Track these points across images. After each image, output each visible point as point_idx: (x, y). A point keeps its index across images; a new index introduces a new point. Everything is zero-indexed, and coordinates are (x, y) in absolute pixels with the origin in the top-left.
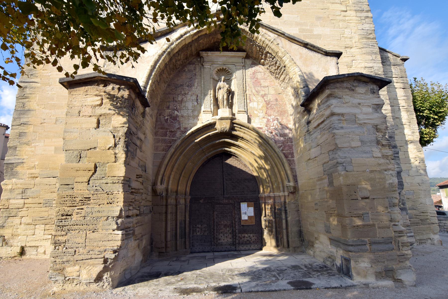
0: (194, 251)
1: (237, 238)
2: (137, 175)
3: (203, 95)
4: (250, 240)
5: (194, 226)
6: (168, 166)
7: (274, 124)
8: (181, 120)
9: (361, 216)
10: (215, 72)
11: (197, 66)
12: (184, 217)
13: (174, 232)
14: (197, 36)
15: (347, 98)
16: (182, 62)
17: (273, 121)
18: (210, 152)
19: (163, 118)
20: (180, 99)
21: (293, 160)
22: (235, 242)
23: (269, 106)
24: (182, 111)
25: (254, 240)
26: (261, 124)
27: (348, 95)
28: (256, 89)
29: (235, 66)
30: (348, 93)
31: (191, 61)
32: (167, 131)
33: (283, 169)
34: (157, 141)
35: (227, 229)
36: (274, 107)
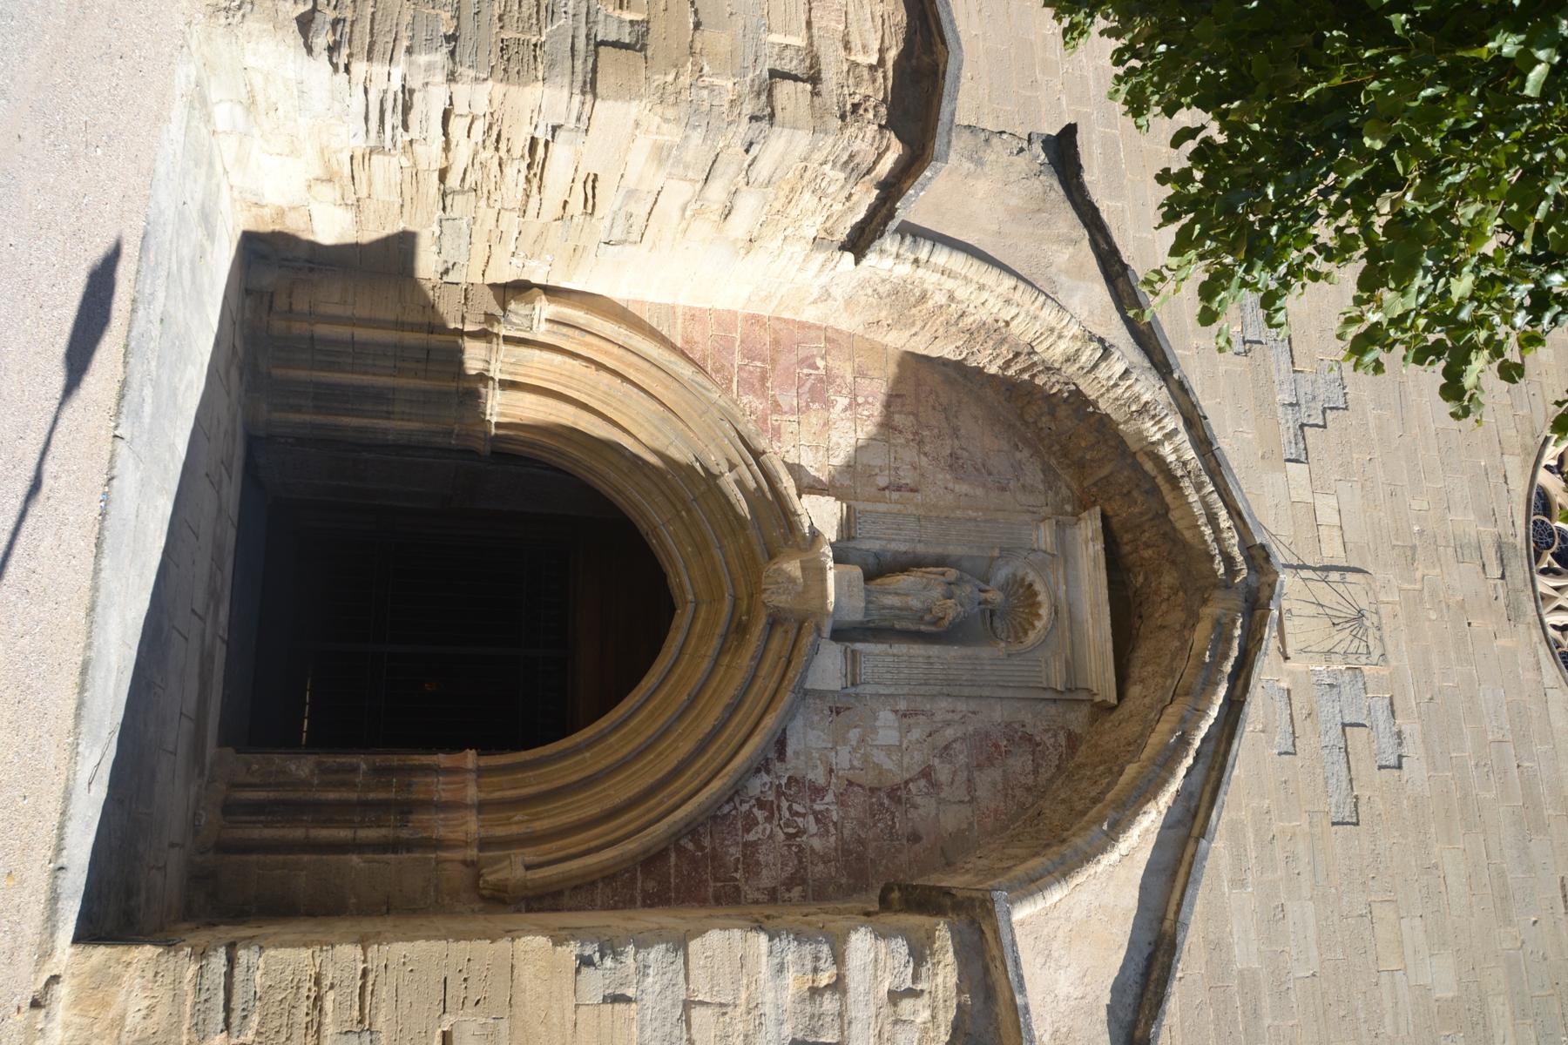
3: (921, 512)
7: (804, 815)
8: (814, 420)
11: (1042, 498)
17: (815, 813)
23: (886, 801)
32: (764, 361)
34: (725, 320)
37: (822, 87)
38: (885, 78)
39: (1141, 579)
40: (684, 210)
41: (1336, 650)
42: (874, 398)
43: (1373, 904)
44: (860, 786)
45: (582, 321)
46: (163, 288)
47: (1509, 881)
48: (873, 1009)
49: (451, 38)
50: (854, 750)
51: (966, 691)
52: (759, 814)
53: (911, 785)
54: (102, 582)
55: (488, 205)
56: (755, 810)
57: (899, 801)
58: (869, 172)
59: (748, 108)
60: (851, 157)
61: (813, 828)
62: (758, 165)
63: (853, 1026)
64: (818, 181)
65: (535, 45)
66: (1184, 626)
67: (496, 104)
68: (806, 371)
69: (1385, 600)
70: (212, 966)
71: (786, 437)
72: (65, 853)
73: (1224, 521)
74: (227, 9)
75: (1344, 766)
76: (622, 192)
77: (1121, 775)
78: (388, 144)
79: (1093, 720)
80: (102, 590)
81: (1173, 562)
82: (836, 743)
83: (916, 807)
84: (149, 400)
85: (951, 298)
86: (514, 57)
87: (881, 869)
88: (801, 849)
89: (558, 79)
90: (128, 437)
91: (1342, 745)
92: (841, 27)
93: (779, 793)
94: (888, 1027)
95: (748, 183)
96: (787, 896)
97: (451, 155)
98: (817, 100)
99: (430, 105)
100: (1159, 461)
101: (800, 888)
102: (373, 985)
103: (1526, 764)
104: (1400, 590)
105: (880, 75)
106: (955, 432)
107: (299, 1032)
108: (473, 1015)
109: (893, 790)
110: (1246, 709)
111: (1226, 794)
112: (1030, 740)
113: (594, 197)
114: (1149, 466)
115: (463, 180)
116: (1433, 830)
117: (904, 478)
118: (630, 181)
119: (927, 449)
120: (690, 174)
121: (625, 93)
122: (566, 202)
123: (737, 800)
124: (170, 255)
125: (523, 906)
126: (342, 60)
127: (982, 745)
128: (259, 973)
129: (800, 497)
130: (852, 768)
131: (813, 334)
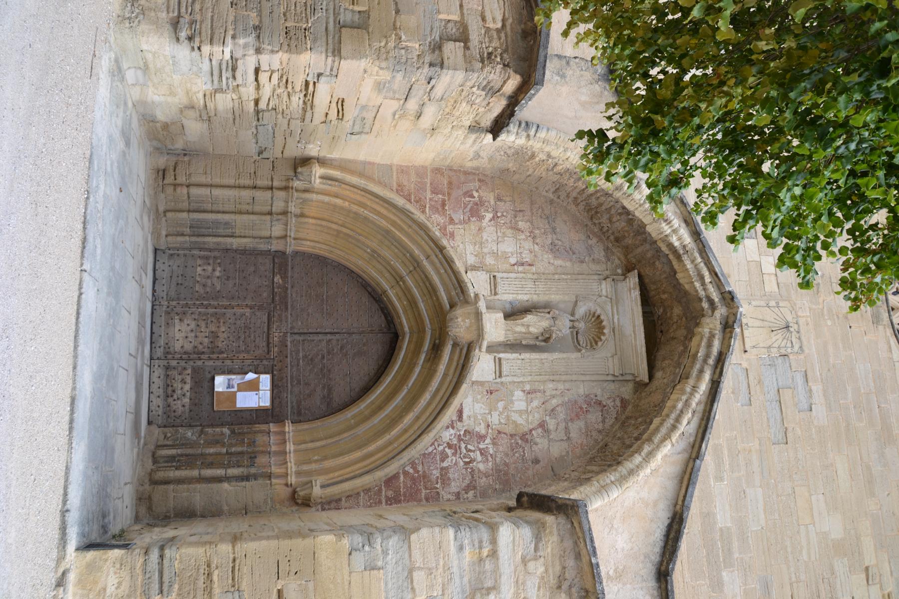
0: (157, 259)
1: (183, 363)
2: (343, 101)
3: (535, 276)
4: (175, 397)
5: (219, 261)
6: (363, 193)
7: (474, 451)
8: (473, 227)
9: (233, 586)
10: (593, 310)
11: (604, 266)
12: (242, 234)
13: (209, 207)
14: (667, 252)
15: (537, 568)
16: (608, 231)
17: (480, 450)
18: (399, 299)
19: (475, 186)
20: (521, 224)
21: (380, 502)
22: (173, 358)
23: (520, 442)
24: (493, 228)
25: (175, 407)
26: (472, 419)
27: (546, 571)
28: (559, 409)
29: (612, 356)
30: (550, 571)
31: (613, 253)
32: (444, 195)
33: (357, 472)
34: (421, 172)
35: (206, 340)
36: (517, 455)
37: (471, 44)
38: (506, 36)
39: (661, 310)
40: (394, 115)
41: (774, 345)
42: (507, 213)
43: (796, 488)
44: (504, 433)
45: (339, 177)
46: (103, 181)
47: (873, 472)
48: (513, 568)
49: (257, 28)
50: (501, 414)
51: (564, 378)
52: (449, 452)
53: (533, 432)
54: (79, 352)
55: (283, 117)
56: (446, 449)
57: (527, 441)
58: (498, 91)
59: (428, 59)
60: (489, 83)
61: (479, 458)
62: (435, 90)
63: (502, 577)
64: (470, 96)
65: (305, 29)
66: (686, 338)
67: (284, 64)
68: (467, 199)
69: (802, 315)
70: (151, 559)
71: (457, 238)
72: (68, 502)
73: (708, 279)
74: (129, 18)
75: (779, 411)
76: (359, 107)
77: (651, 424)
78: (224, 87)
79: (636, 391)
80: (79, 357)
81: (679, 302)
82: (491, 411)
83: (536, 444)
84: (99, 246)
85: (549, 156)
86: (294, 37)
87: (518, 479)
88: (473, 470)
89: (319, 48)
90: (88, 270)
91: (778, 399)
92: (480, 8)
93: (460, 439)
94: (521, 577)
95: (430, 100)
96: (465, 496)
97: (260, 92)
98: (468, 53)
99: (248, 63)
100: (670, 246)
101: (473, 492)
102: (239, 566)
103: (883, 406)
104: (810, 309)
105: (503, 35)
106: (554, 230)
107: (200, 593)
108: (294, 580)
109: (523, 435)
110: (721, 385)
111: (710, 434)
112: (600, 404)
113: (343, 110)
114: (664, 248)
115: (268, 104)
116: (829, 445)
117: (526, 258)
118: (363, 101)
119: (538, 241)
120: (397, 96)
121: (358, 55)
122: (327, 114)
123: (436, 444)
124: (106, 161)
125: (319, 507)
126: (197, 44)
127: (573, 408)
128: (177, 562)
129: (466, 273)
130: (500, 423)
131: (471, 177)
